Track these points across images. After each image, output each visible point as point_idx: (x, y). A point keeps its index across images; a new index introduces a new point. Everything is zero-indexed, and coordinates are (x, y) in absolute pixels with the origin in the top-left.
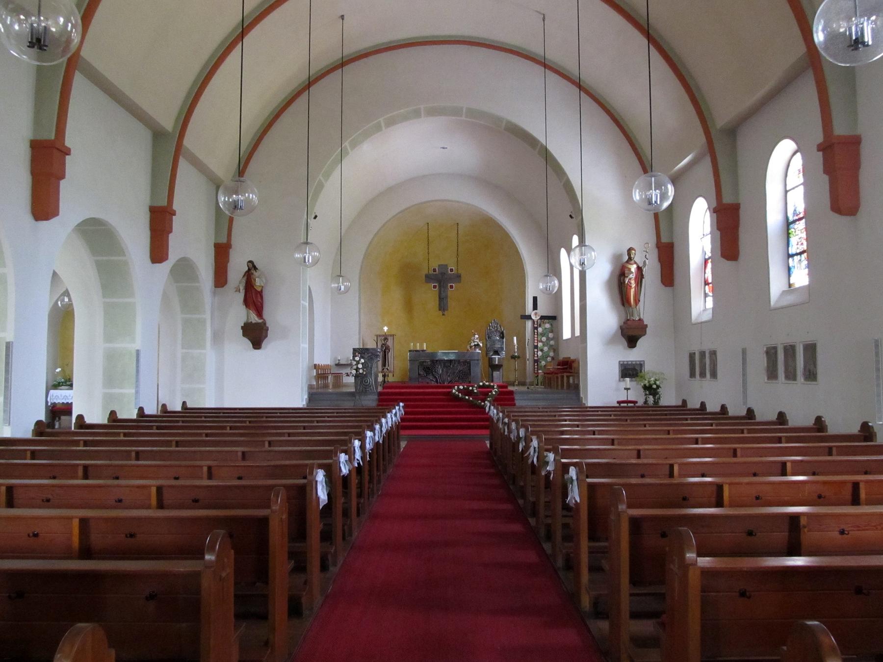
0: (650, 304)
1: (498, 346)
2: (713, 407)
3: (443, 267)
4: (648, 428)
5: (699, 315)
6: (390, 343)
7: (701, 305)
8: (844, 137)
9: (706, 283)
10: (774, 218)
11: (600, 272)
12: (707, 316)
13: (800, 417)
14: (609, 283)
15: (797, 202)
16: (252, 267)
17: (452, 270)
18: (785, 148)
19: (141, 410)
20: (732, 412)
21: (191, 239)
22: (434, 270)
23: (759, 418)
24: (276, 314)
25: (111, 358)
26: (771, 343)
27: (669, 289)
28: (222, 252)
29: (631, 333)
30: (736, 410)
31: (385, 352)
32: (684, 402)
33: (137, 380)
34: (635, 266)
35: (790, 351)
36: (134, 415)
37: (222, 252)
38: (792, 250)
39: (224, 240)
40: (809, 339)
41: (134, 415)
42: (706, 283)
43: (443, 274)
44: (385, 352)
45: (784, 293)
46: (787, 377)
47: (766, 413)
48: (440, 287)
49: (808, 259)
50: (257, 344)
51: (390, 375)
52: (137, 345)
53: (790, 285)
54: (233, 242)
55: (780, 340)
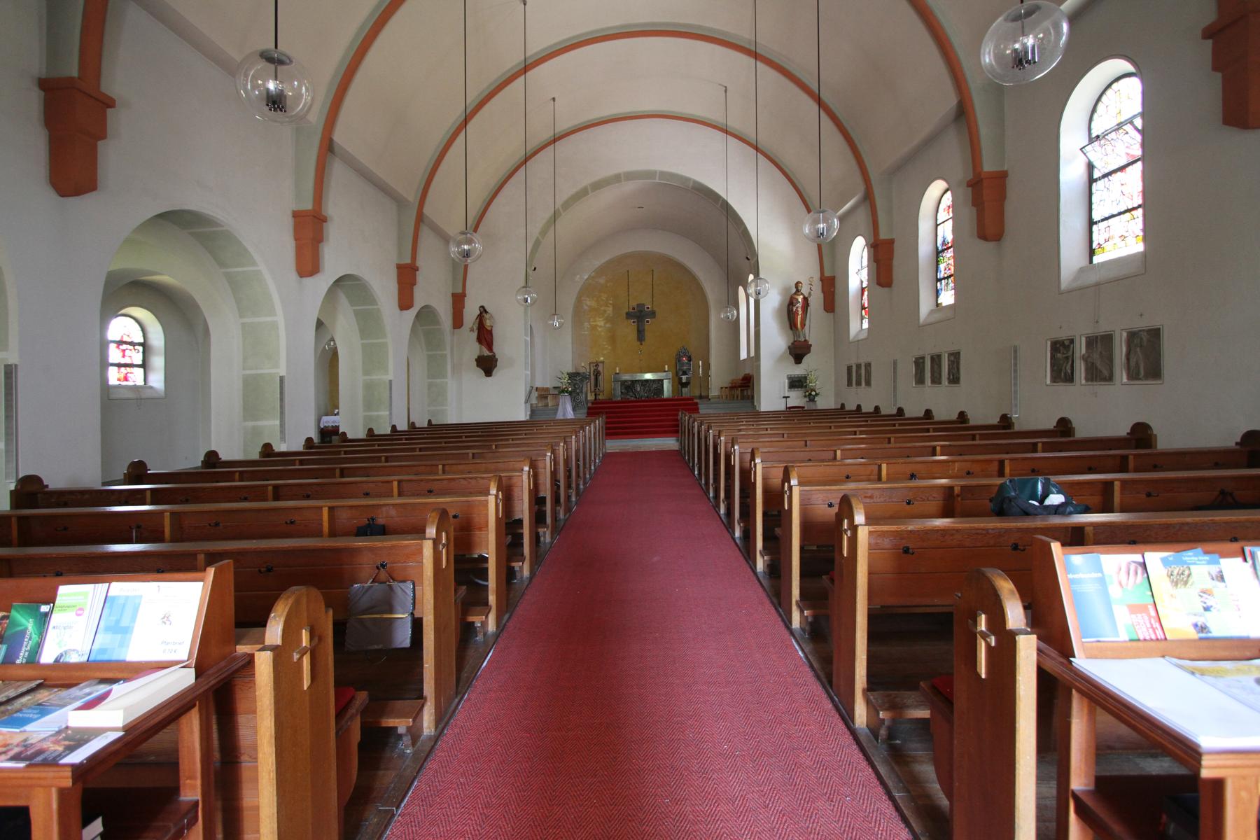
0: (815, 328)
2: (941, 414)
3: (641, 306)
4: (833, 430)
5: (857, 334)
6: (600, 369)
7: (858, 325)
9: (863, 308)
10: (925, 248)
11: (772, 301)
12: (864, 335)
13: (945, 411)
14: (779, 310)
15: (946, 232)
16: (483, 310)
18: (937, 187)
19: (394, 427)
20: (884, 411)
21: (432, 290)
23: (883, 413)
24: (502, 348)
25: (369, 387)
26: (921, 353)
27: (831, 315)
28: (458, 301)
29: (799, 352)
30: (888, 409)
32: (843, 405)
33: (282, 413)
35: (936, 359)
36: (388, 431)
37: (458, 301)
38: (941, 275)
40: (954, 348)
41: (388, 431)
42: (863, 308)
45: (932, 312)
46: (933, 382)
47: (914, 410)
49: (955, 282)
50: (488, 373)
52: (390, 377)
53: (938, 305)
55: (928, 350)
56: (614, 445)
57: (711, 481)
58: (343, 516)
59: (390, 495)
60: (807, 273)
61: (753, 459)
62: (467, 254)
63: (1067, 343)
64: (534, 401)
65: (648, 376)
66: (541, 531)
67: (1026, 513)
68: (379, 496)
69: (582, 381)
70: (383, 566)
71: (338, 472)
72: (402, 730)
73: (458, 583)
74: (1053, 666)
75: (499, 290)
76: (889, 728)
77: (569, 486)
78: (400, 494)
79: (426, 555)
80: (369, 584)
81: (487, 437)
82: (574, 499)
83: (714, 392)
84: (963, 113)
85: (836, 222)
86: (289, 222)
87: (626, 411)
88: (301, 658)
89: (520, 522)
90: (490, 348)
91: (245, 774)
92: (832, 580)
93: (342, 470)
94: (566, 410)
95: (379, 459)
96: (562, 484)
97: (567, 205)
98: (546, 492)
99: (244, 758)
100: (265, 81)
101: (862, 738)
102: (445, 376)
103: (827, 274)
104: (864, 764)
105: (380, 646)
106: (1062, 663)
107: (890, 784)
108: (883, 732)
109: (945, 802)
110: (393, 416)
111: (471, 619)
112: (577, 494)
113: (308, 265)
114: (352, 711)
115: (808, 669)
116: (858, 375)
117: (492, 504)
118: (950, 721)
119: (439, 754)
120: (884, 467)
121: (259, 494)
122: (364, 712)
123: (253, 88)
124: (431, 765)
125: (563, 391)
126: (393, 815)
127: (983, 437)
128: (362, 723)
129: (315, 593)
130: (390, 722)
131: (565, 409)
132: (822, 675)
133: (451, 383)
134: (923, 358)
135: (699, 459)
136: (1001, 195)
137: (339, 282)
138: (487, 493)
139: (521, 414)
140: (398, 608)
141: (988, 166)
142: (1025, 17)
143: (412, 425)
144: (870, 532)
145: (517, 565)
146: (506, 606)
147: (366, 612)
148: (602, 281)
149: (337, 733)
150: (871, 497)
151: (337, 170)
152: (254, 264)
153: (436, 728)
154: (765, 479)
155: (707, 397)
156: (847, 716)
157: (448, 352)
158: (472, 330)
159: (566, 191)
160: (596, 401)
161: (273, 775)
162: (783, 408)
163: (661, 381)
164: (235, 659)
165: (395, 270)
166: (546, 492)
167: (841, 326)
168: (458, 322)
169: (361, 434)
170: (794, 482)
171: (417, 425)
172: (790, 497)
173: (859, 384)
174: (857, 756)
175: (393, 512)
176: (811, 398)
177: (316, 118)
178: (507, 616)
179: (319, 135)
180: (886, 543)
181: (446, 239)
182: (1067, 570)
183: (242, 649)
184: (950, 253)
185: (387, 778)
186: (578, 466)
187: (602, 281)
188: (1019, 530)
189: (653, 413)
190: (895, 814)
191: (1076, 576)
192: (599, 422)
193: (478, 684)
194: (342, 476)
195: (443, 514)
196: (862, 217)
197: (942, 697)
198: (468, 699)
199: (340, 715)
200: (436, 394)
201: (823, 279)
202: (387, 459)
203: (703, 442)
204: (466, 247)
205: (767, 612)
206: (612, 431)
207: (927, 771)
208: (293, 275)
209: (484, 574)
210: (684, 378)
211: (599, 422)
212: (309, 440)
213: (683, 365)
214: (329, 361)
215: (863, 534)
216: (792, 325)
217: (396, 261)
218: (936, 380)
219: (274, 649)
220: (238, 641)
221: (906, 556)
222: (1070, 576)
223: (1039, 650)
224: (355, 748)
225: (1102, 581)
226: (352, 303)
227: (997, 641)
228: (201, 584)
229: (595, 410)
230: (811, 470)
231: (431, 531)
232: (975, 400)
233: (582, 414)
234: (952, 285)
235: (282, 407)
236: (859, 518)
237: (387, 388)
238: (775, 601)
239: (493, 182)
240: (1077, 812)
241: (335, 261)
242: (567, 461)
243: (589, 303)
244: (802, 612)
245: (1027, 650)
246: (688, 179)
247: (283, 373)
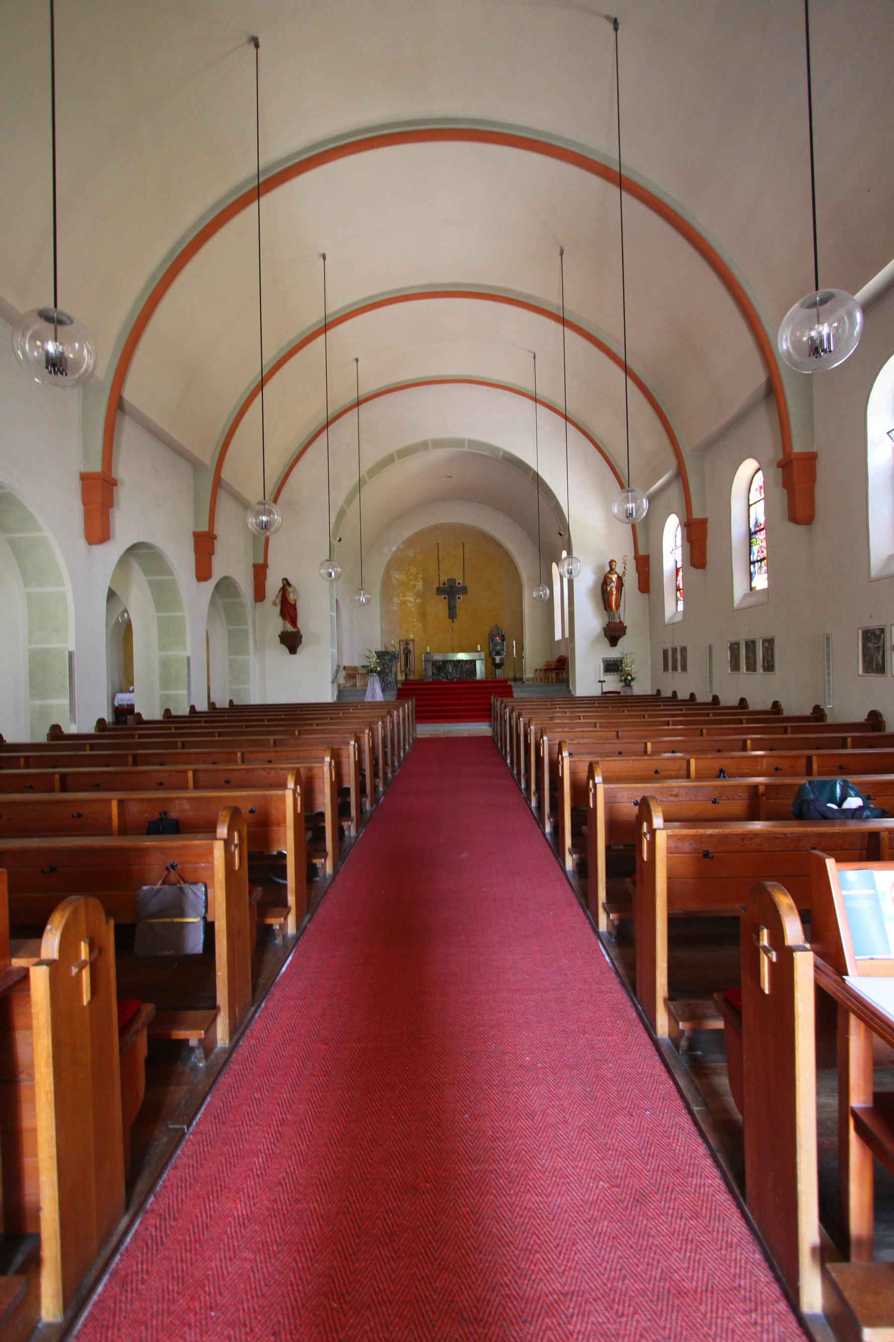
1: (498, 648)
6: (411, 647)
7: (673, 607)
9: (678, 589)
10: (738, 530)
11: (586, 582)
12: (679, 618)
13: (759, 702)
14: (593, 590)
15: (759, 513)
16: (286, 583)
18: (749, 466)
19: (192, 708)
21: (233, 561)
22: (444, 584)
25: (165, 664)
26: (734, 639)
27: (646, 595)
28: (260, 571)
30: (704, 697)
32: (659, 691)
33: (72, 691)
34: (616, 576)
35: (751, 645)
37: (260, 571)
38: (754, 558)
40: (768, 635)
42: (678, 589)
43: (452, 587)
45: (746, 596)
46: (748, 669)
47: (729, 699)
48: (450, 598)
50: (293, 650)
51: (412, 674)
52: (188, 652)
53: (751, 589)
54: (269, 562)
55: (742, 637)
56: (426, 730)
57: (523, 772)
58: (134, 810)
59: (185, 788)
60: (621, 552)
61: (560, 752)
62: (265, 526)
63: (877, 632)
64: (342, 681)
65: (462, 656)
66: (345, 824)
67: (825, 816)
68: (174, 788)
69: (391, 660)
70: (173, 867)
71: (130, 759)
72: (193, 1042)
73: (253, 882)
74: (829, 985)
75: (303, 560)
76: (690, 1039)
77: (375, 775)
78: (196, 787)
79: (218, 855)
80: (158, 886)
81: (294, 718)
82: (381, 789)
83: (529, 674)
84: (772, 390)
85: (645, 503)
86: (76, 485)
87: (437, 692)
88: (80, 971)
89: (322, 815)
90: (294, 623)
91: (24, 1094)
92: (634, 883)
93: (135, 757)
94: (375, 692)
95: (174, 745)
96: (368, 773)
97: (373, 472)
98: (350, 782)
99: (23, 1076)
100: (44, 341)
101: (663, 1049)
102: (246, 653)
104: (665, 1076)
105: (172, 952)
106: (836, 981)
107: (689, 1097)
108: (684, 1043)
109: (739, 1117)
110: (190, 697)
111: (269, 921)
112: (385, 783)
113: (98, 529)
114: (138, 1024)
115: (613, 975)
116: (673, 660)
117: (289, 800)
118: (739, 1034)
119: (233, 1068)
120: (693, 762)
121: (44, 784)
122: (151, 1025)
123: (31, 350)
124: (225, 1079)
125: (371, 671)
126: (184, 1134)
127: (795, 730)
128: (149, 1036)
129: (94, 903)
130: (181, 1034)
131: (374, 690)
132: (627, 982)
133: (253, 660)
134: (738, 644)
135: (511, 746)
136: (811, 477)
137: (133, 550)
138: (284, 786)
139: (327, 695)
140: (190, 912)
141: (798, 447)
142: (820, 305)
143: (212, 705)
144: (669, 836)
145: (318, 862)
146: (306, 907)
147: (160, 914)
148: (411, 554)
149: (121, 1050)
150: (677, 795)
151: (128, 431)
152: (39, 529)
153: (231, 1039)
154: (573, 773)
155: (521, 679)
156: (650, 1026)
157: (250, 626)
158: (274, 604)
159: (371, 458)
160: (406, 682)
161: (51, 1097)
162: (598, 693)
163: (473, 662)
164: (10, 973)
165: (192, 538)
166: (350, 782)
167: (655, 607)
168: (260, 594)
169: (158, 715)
170: (598, 779)
171: (218, 706)
172: (595, 795)
173: (675, 668)
174: (659, 1068)
175: (186, 806)
176: (627, 683)
177: (105, 374)
178: (307, 918)
179: (108, 392)
180: (686, 846)
181: (245, 505)
182: (842, 886)
183: (18, 962)
184: (762, 536)
185: (179, 1093)
186: (385, 754)
187: (411, 554)
188: (818, 835)
189: (460, 704)
190: (693, 1128)
191: (850, 893)
192: (409, 705)
193: (277, 993)
194: (135, 764)
195: (235, 814)
196: (675, 494)
197: (732, 1008)
198: (266, 1007)
199: (124, 1029)
200: (238, 673)
201: (637, 558)
202: (184, 745)
203: (515, 729)
204: (264, 518)
205: (575, 914)
206: (423, 715)
207: (723, 1082)
208: (83, 542)
209: (282, 871)
210: (498, 659)
211: (409, 705)
212: (101, 721)
213: (496, 644)
214: (122, 634)
215: (661, 838)
216: (607, 605)
217: (193, 529)
218: (751, 667)
219: (50, 963)
220: (14, 954)
221: (707, 863)
222: (843, 893)
223: (817, 967)
224: (141, 1064)
225: (875, 898)
226: (146, 573)
227: (778, 957)
229: (406, 691)
230: (618, 765)
231: (222, 831)
232: (786, 689)
233: (392, 696)
234: (764, 568)
235: (71, 684)
236: (658, 821)
237: (186, 665)
238: (583, 902)
239: (294, 448)
240: (857, 1129)
241: (127, 527)
242: (373, 750)
243: (398, 576)
244: (608, 916)
245: (805, 966)
246: (496, 449)
247: (72, 647)
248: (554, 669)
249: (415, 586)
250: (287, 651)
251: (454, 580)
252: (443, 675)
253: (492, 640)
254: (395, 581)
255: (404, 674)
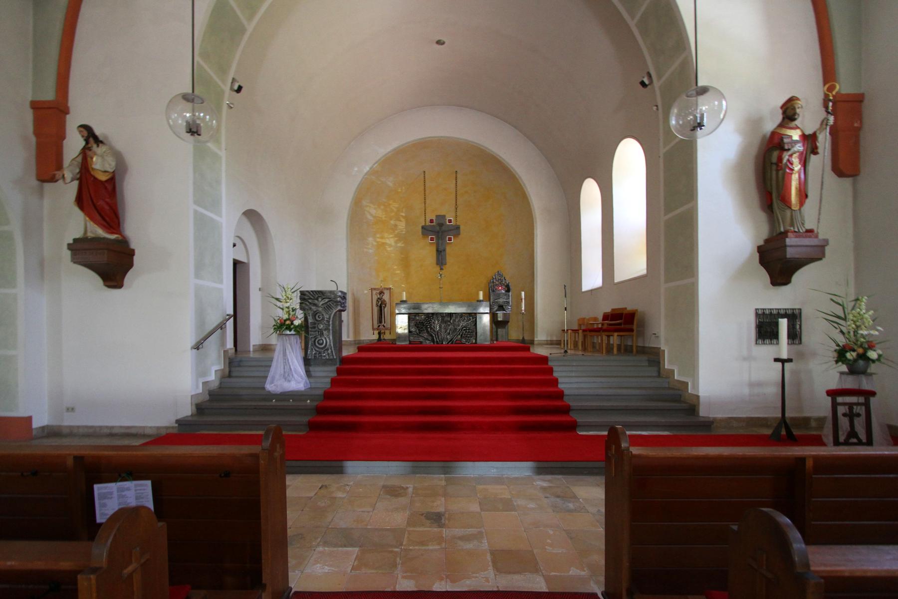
1: (501, 301)
6: (386, 297)
8: (848, 95)
14: (738, 167)
17: (450, 221)
22: (432, 221)
24: (141, 226)
27: (847, 182)
31: (381, 307)
39: (49, 94)
43: (441, 225)
44: (381, 307)
48: (438, 238)
51: (387, 332)
54: (71, 103)
103: (844, 86)
148: (390, 182)
228: (616, 281)
243: (373, 211)
248: (605, 331)
249: (396, 226)
250: (99, 281)
251: (444, 216)
252: (426, 335)
253: (493, 291)
254: (369, 217)
255: (376, 332)
